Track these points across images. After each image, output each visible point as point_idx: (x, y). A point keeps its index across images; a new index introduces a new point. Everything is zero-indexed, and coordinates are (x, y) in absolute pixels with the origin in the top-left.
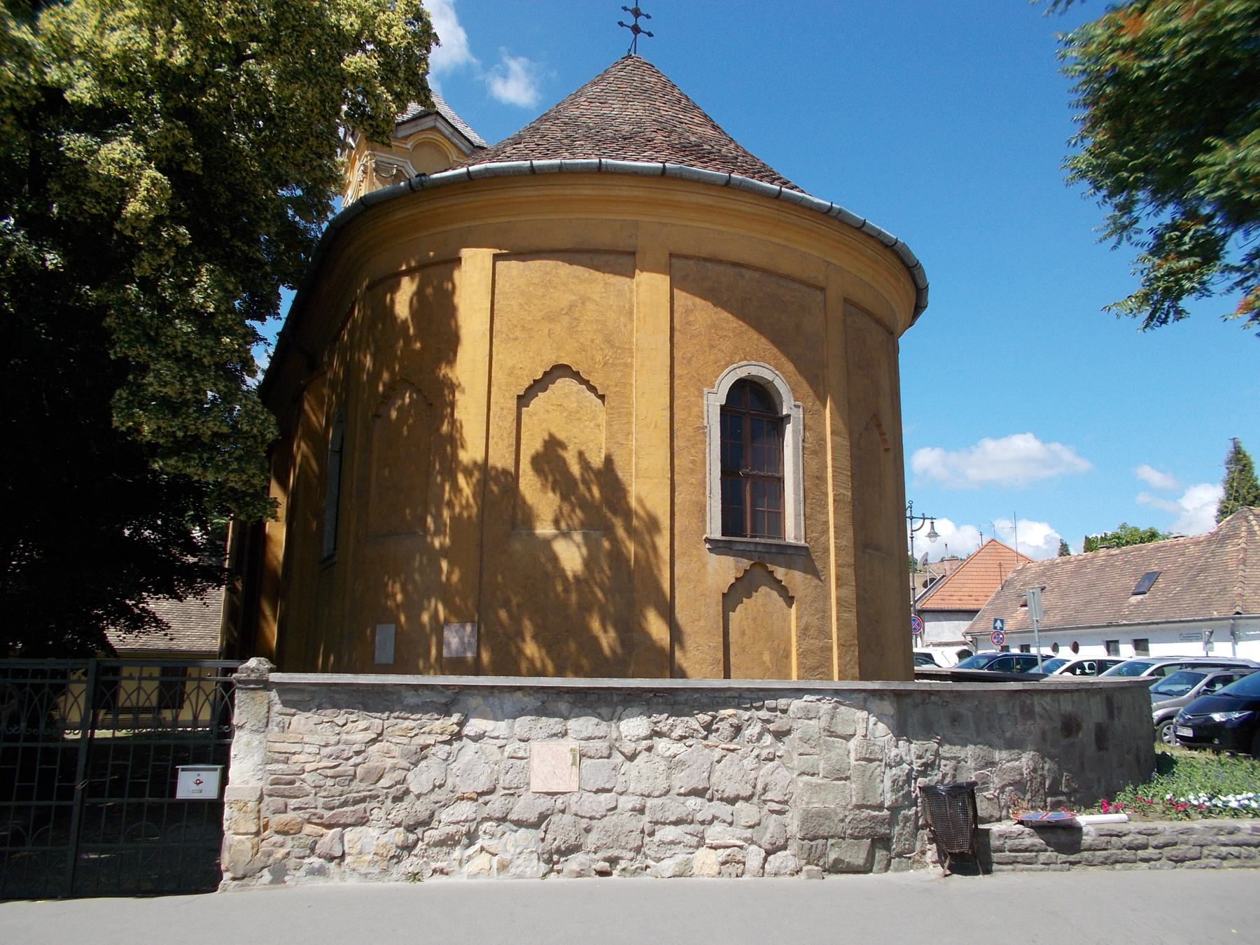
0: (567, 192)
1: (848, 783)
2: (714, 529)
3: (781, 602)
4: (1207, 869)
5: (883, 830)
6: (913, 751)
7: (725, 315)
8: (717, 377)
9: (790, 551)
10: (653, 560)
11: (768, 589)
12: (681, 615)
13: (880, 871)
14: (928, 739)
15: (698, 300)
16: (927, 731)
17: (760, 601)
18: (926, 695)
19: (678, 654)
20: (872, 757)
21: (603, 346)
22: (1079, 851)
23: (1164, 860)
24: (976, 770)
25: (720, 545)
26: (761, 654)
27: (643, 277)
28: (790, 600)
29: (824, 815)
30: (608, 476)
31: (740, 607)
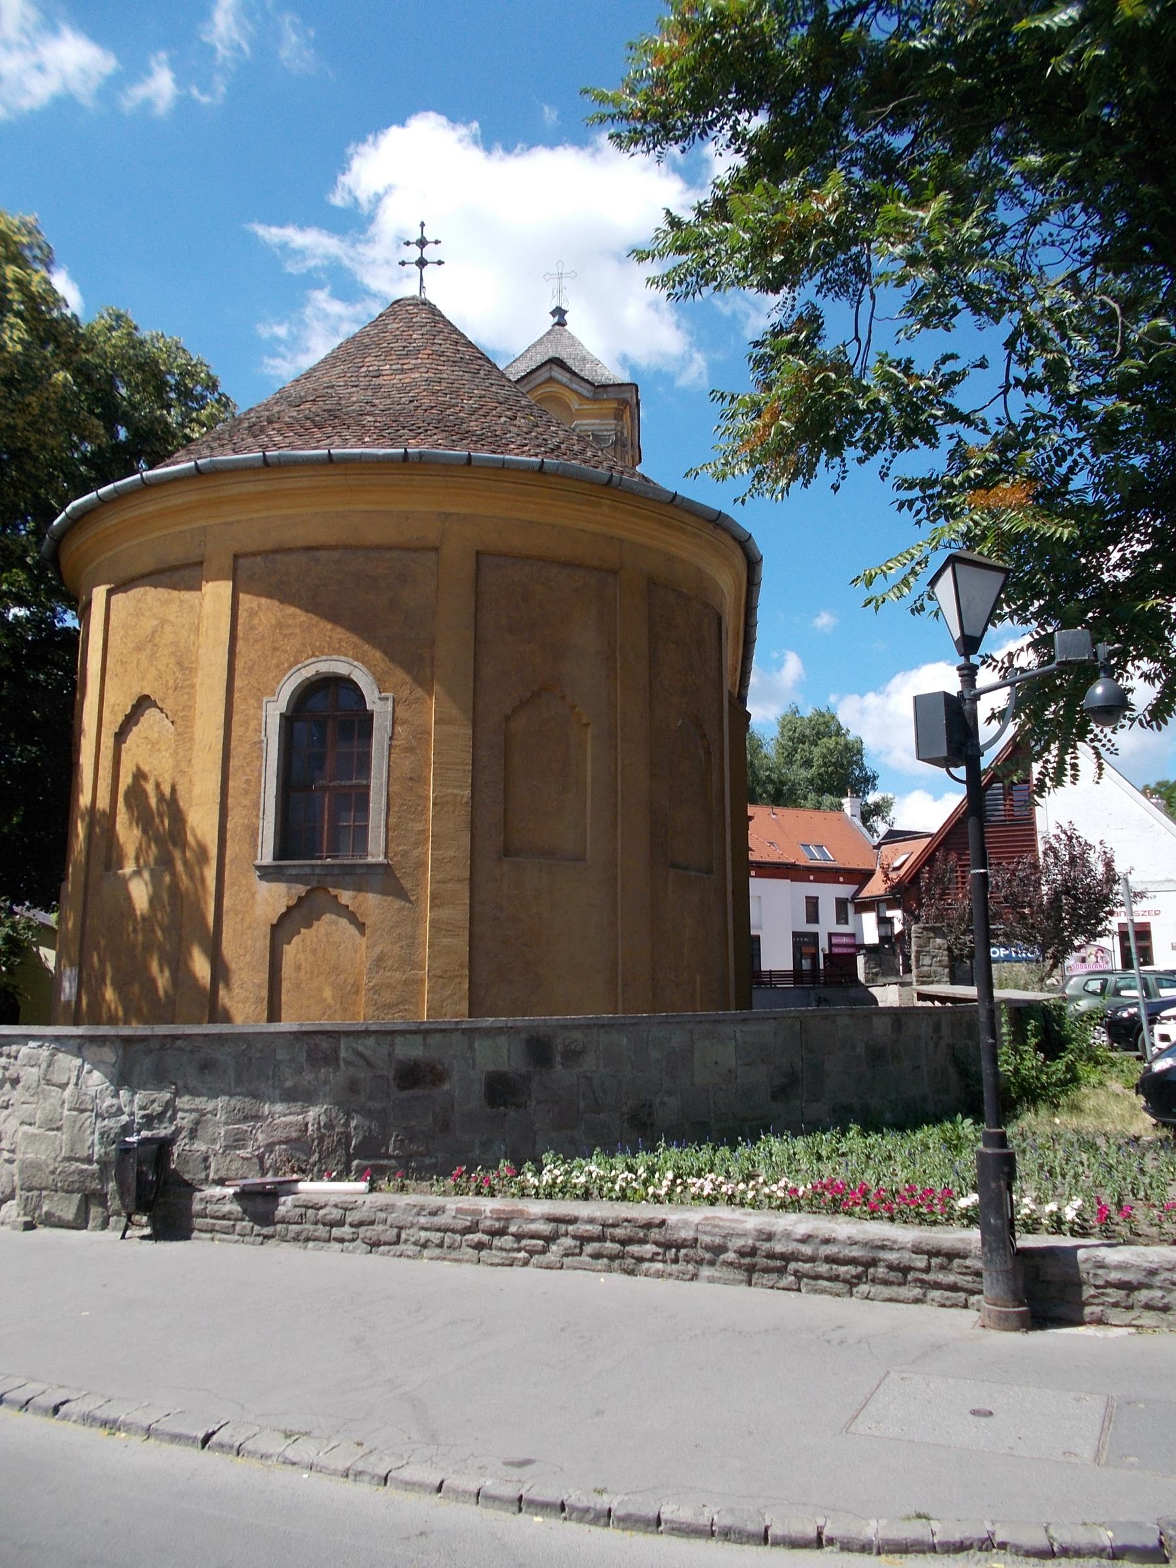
0: (136, 513)
1: (59, 1134)
2: (266, 856)
3: (353, 930)
4: (402, 1259)
5: (95, 1185)
6: (136, 1101)
7: (292, 610)
8: (278, 683)
9: (359, 871)
10: (201, 893)
11: (334, 917)
12: (228, 949)
13: (94, 1229)
14: (160, 1089)
15: (263, 601)
16: (159, 1079)
17: (322, 930)
18: (169, 1040)
19: (222, 992)
20: (82, 1107)
21: (175, 670)
22: (275, 1224)
23: (359, 1242)
24: (226, 1123)
25: (270, 871)
26: (320, 990)
27: (208, 587)
28: (361, 927)
29: (37, 1166)
30: (173, 807)
31: (296, 940)
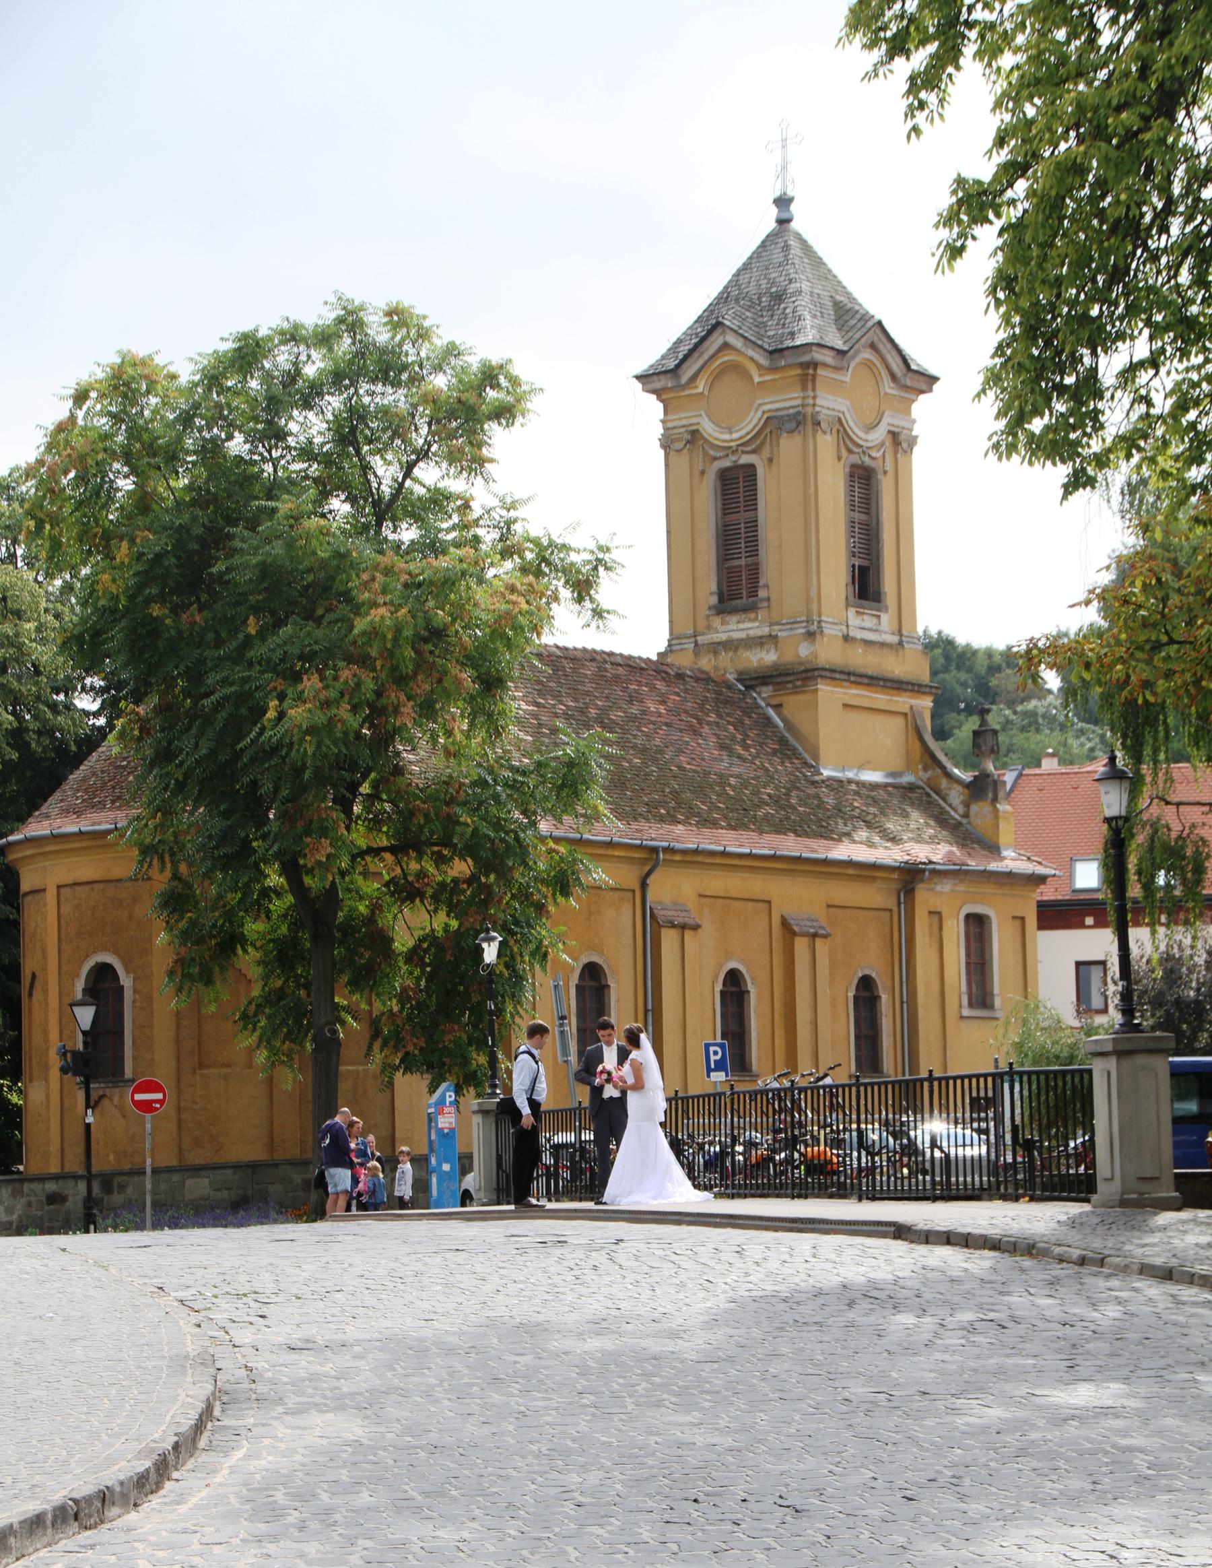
26: (108, 1155)
